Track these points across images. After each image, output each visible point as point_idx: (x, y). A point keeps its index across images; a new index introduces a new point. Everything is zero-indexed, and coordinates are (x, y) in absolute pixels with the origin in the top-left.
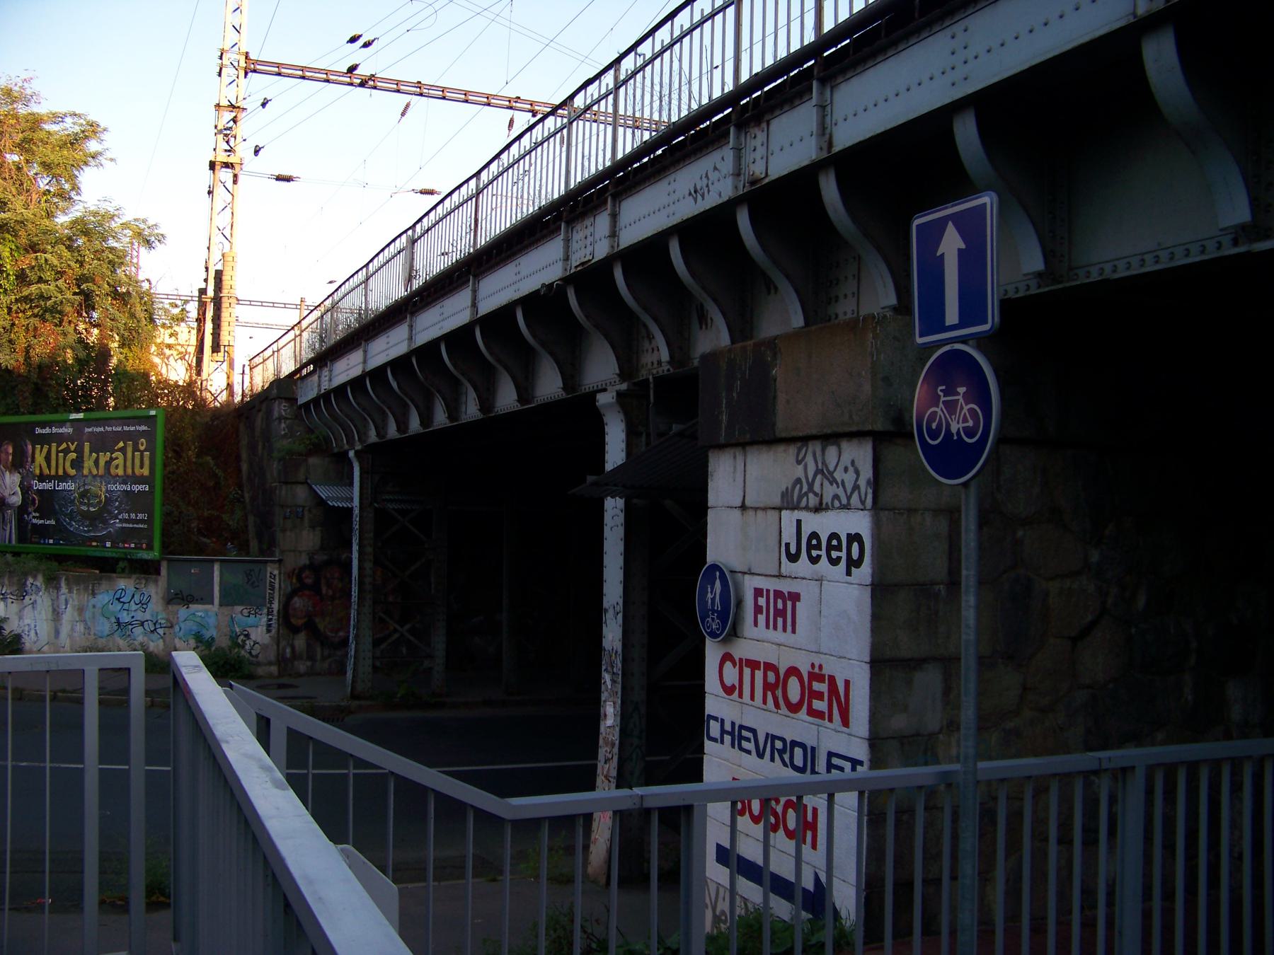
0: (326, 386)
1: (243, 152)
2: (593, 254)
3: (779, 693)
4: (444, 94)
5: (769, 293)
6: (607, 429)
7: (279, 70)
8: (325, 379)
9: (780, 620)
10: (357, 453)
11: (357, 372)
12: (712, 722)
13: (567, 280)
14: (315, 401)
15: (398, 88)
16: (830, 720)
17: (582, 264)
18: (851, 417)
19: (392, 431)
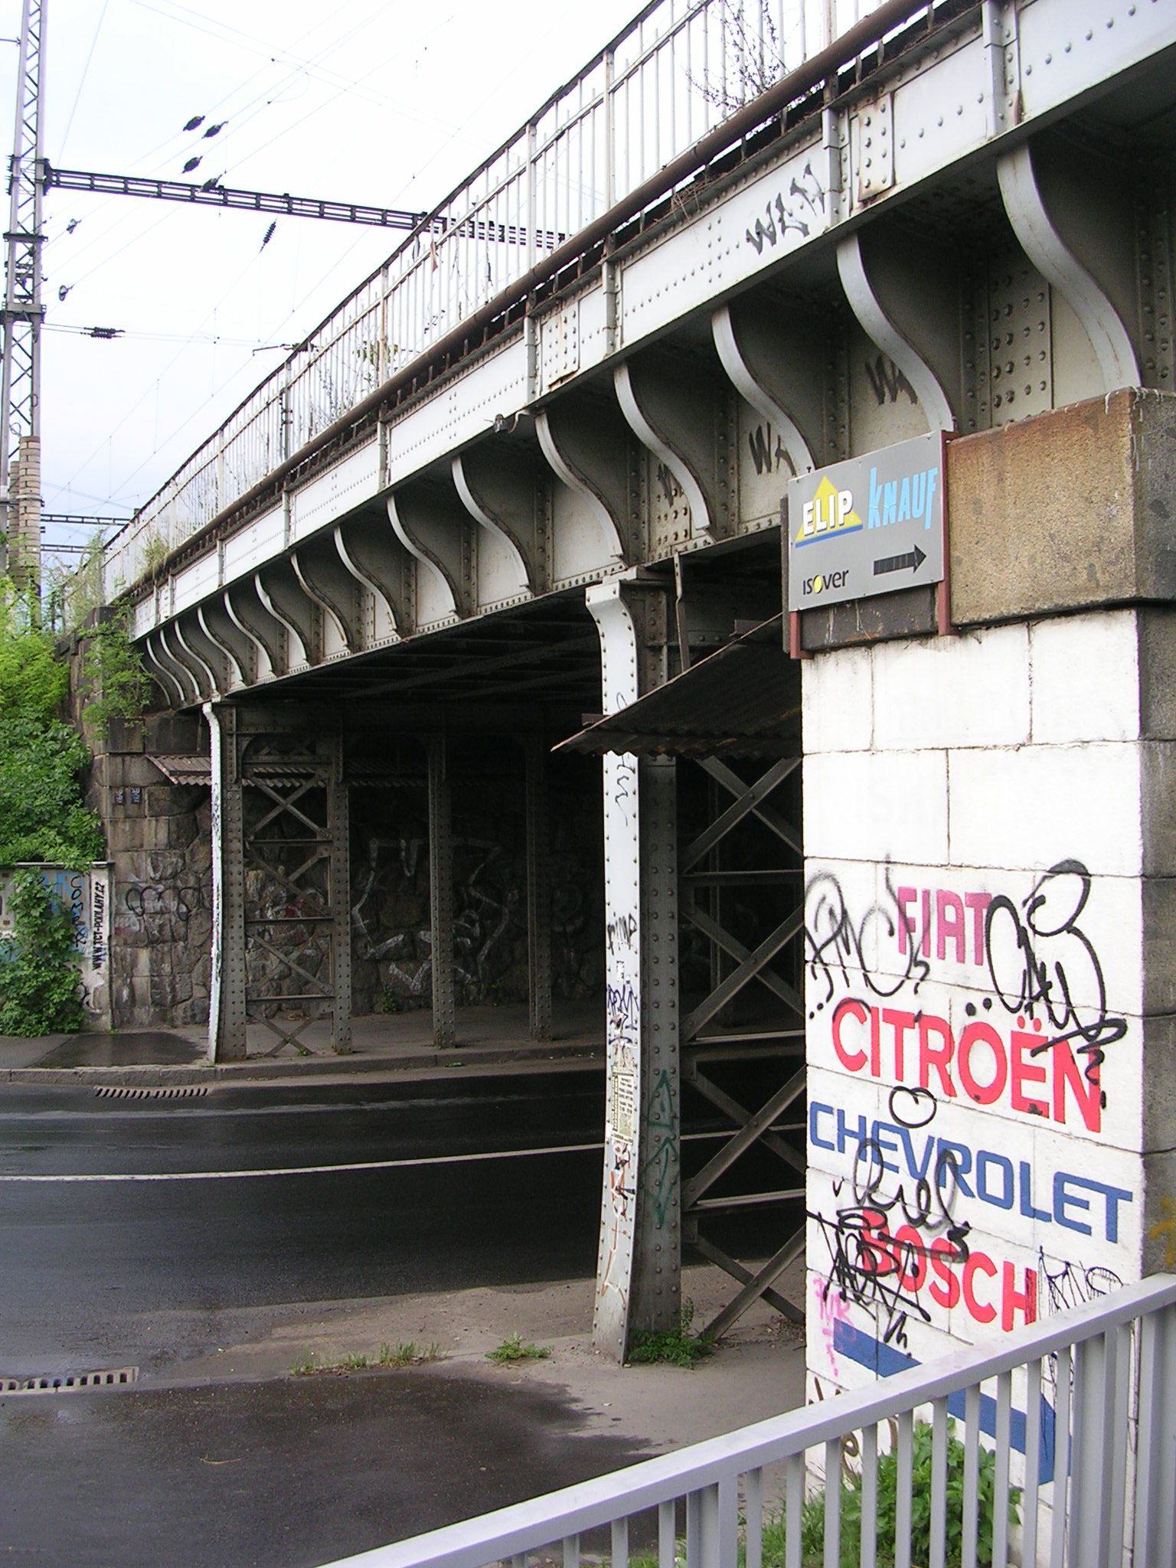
0: (166, 613)
1: (48, 296)
2: (577, 362)
3: (953, 1067)
4: (322, 210)
5: (882, 402)
6: (604, 643)
7: (92, 182)
8: (165, 604)
9: (951, 942)
10: (214, 706)
11: (210, 587)
12: (822, 1116)
13: (534, 409)
14: (153, 635)
15: (257, 202)
16: (1060, 1118)
17: (561, 379)
18: (1091, 575)
19: (266, 674)
